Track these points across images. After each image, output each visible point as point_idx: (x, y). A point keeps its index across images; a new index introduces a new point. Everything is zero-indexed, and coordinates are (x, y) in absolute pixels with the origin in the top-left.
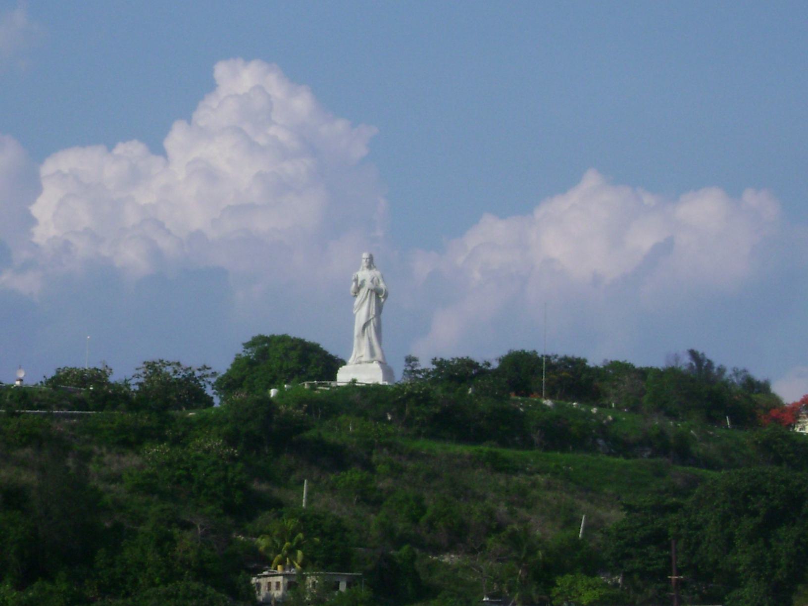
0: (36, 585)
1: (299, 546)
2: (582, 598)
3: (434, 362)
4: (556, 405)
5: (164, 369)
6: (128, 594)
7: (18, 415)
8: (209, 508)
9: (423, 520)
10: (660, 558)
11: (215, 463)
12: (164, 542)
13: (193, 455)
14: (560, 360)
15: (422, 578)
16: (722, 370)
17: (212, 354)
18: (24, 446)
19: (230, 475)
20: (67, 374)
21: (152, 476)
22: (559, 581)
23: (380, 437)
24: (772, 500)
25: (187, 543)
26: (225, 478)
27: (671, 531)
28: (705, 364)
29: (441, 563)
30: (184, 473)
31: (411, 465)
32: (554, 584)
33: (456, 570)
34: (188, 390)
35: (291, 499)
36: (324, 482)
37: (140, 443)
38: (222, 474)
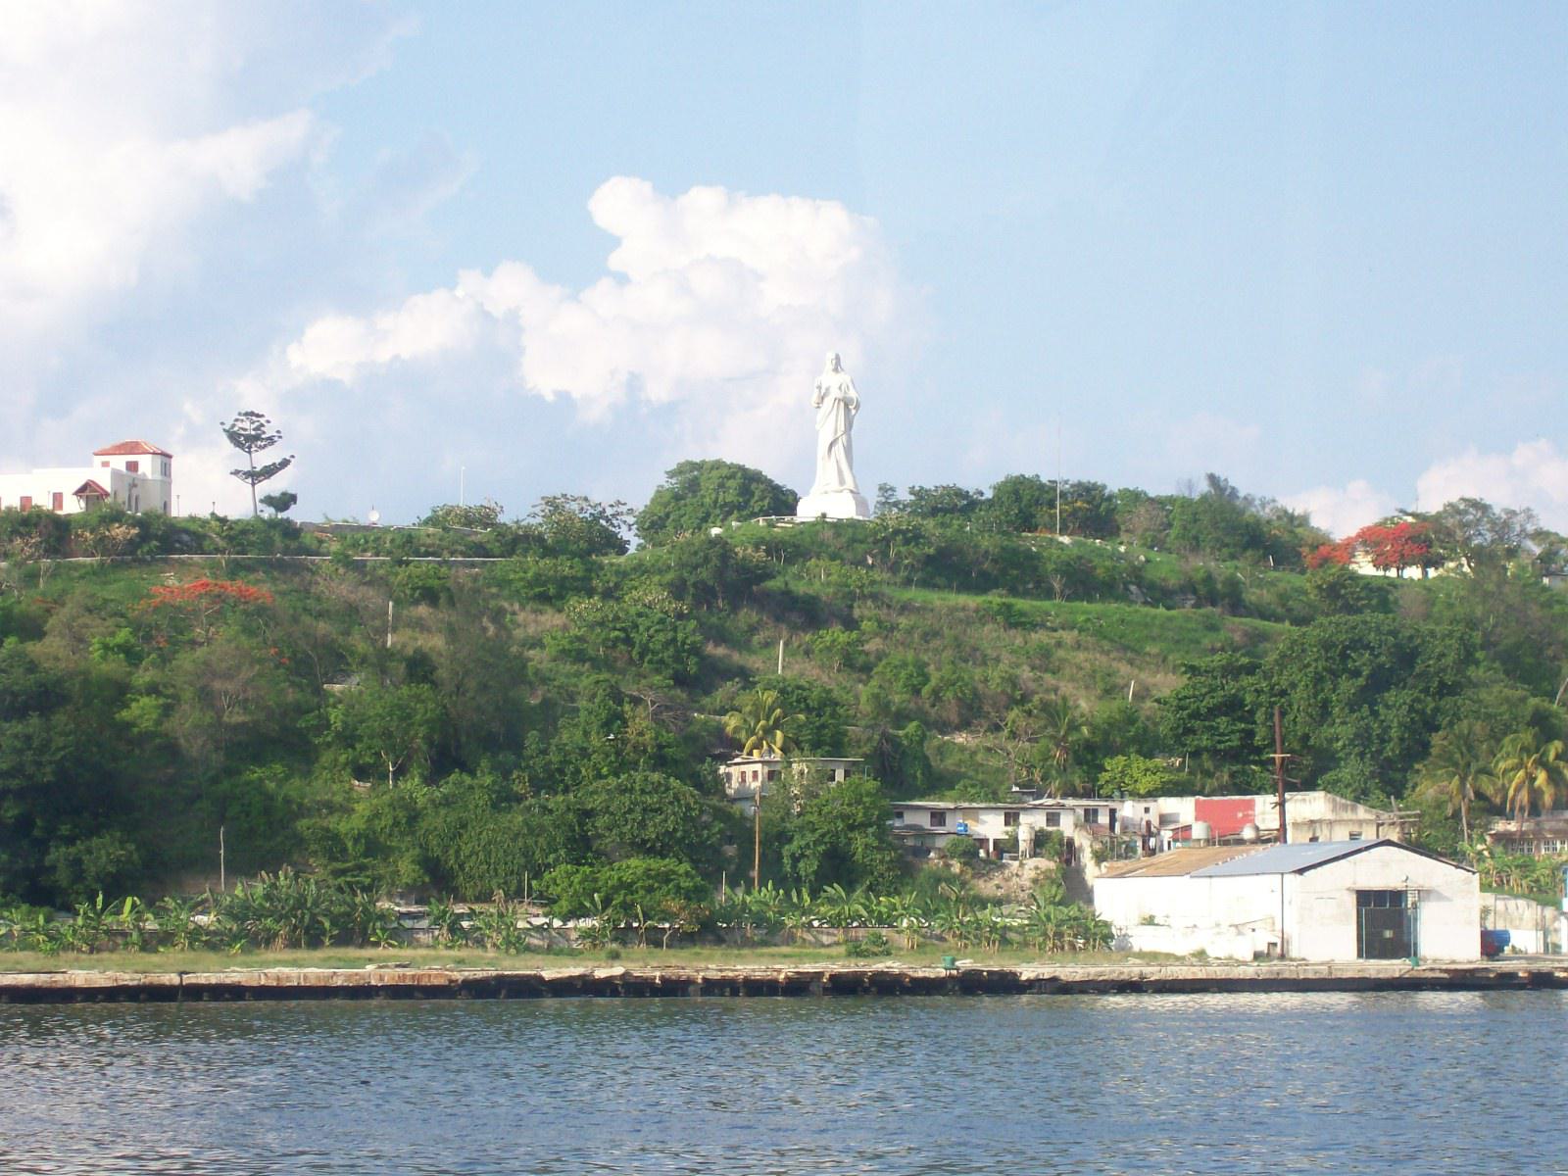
0: (453, 777)
1: (777, 725)
2: (1138, 785)
3: (912, 491)
4: (1074, 543)
5: (567, 506)
6: (566, 791)
7: (408, 563)
8: (657, 679)
9: (926, 691)
10: (1233, 732)
11: (662, 621)
12: (614, 721)
13: (633, 611)
14: (1072, 486)
15: (933, 764)
16: (1249, 501)
17: (625, 488)
18: (416, 602)
19: (680, 636)
20: (448, 513)
21: (581, 639)
22: (1108, 763)
23: (863, 586)
24: (1377, 656)
25: (640, 725)
26: (674, 640)
27: (1248, 699)
28: (1227, 492)
29: (955, 744)
30: (622, 635)
31: (904, 622)
32: (1102, 769)
33: (974, 753)
34: (598, 538)
35: (757, 666)
36: (796, 644)
37: (561, 597)
38: (670, 635)
